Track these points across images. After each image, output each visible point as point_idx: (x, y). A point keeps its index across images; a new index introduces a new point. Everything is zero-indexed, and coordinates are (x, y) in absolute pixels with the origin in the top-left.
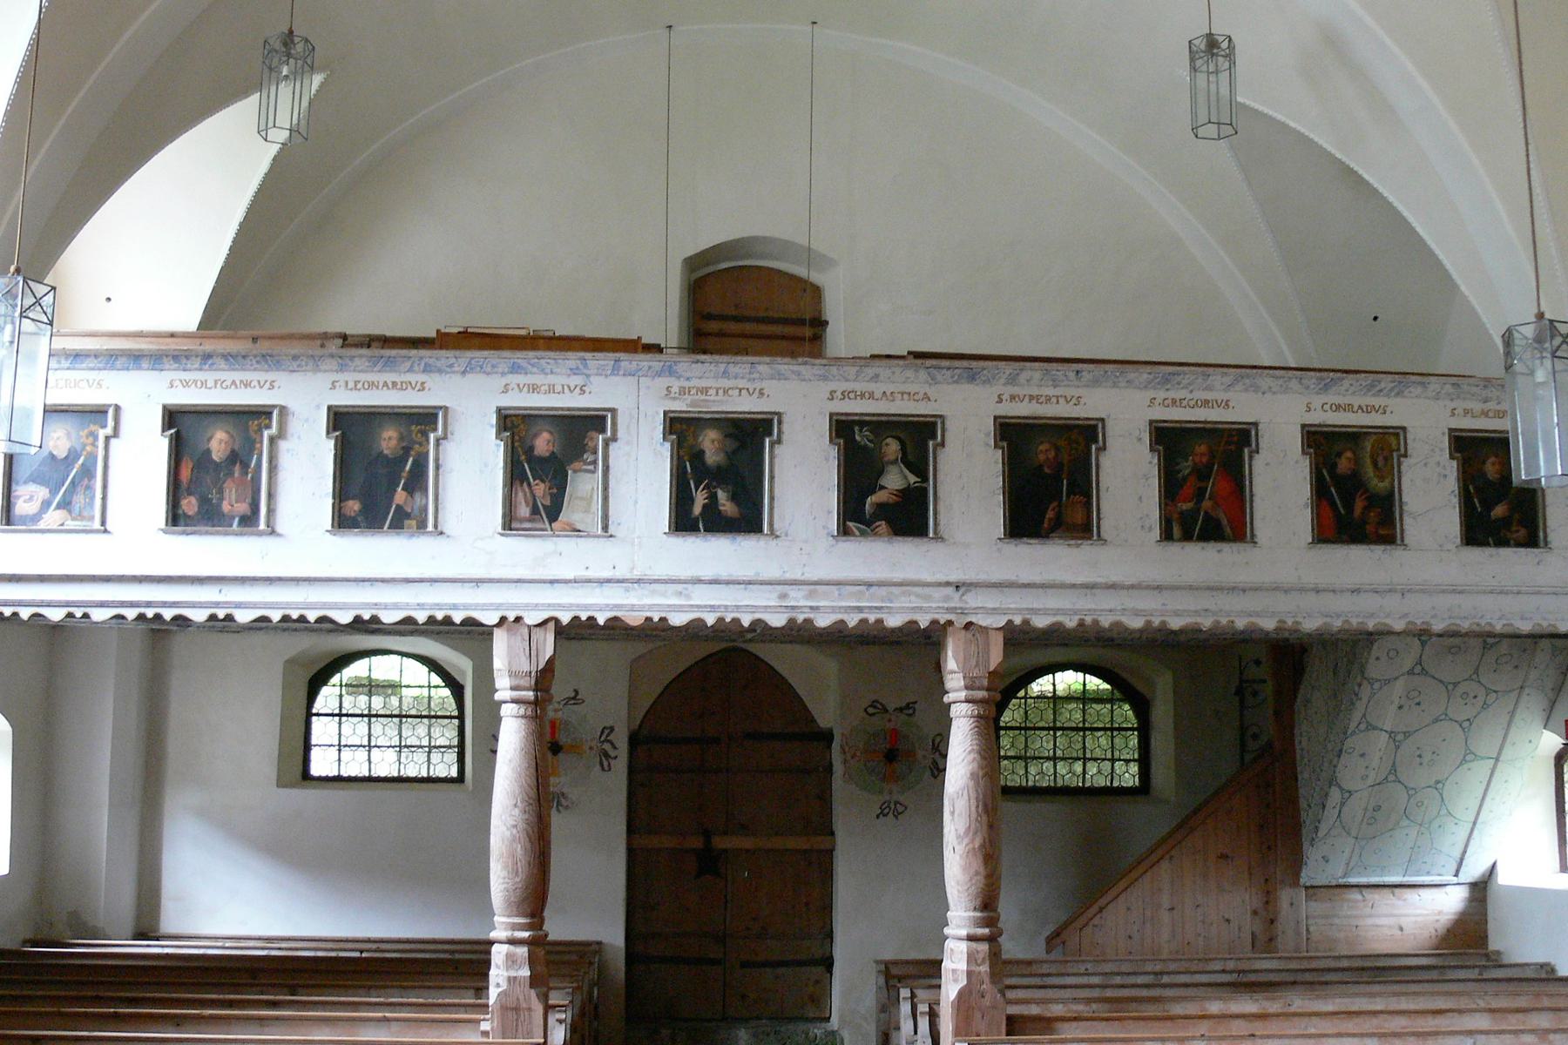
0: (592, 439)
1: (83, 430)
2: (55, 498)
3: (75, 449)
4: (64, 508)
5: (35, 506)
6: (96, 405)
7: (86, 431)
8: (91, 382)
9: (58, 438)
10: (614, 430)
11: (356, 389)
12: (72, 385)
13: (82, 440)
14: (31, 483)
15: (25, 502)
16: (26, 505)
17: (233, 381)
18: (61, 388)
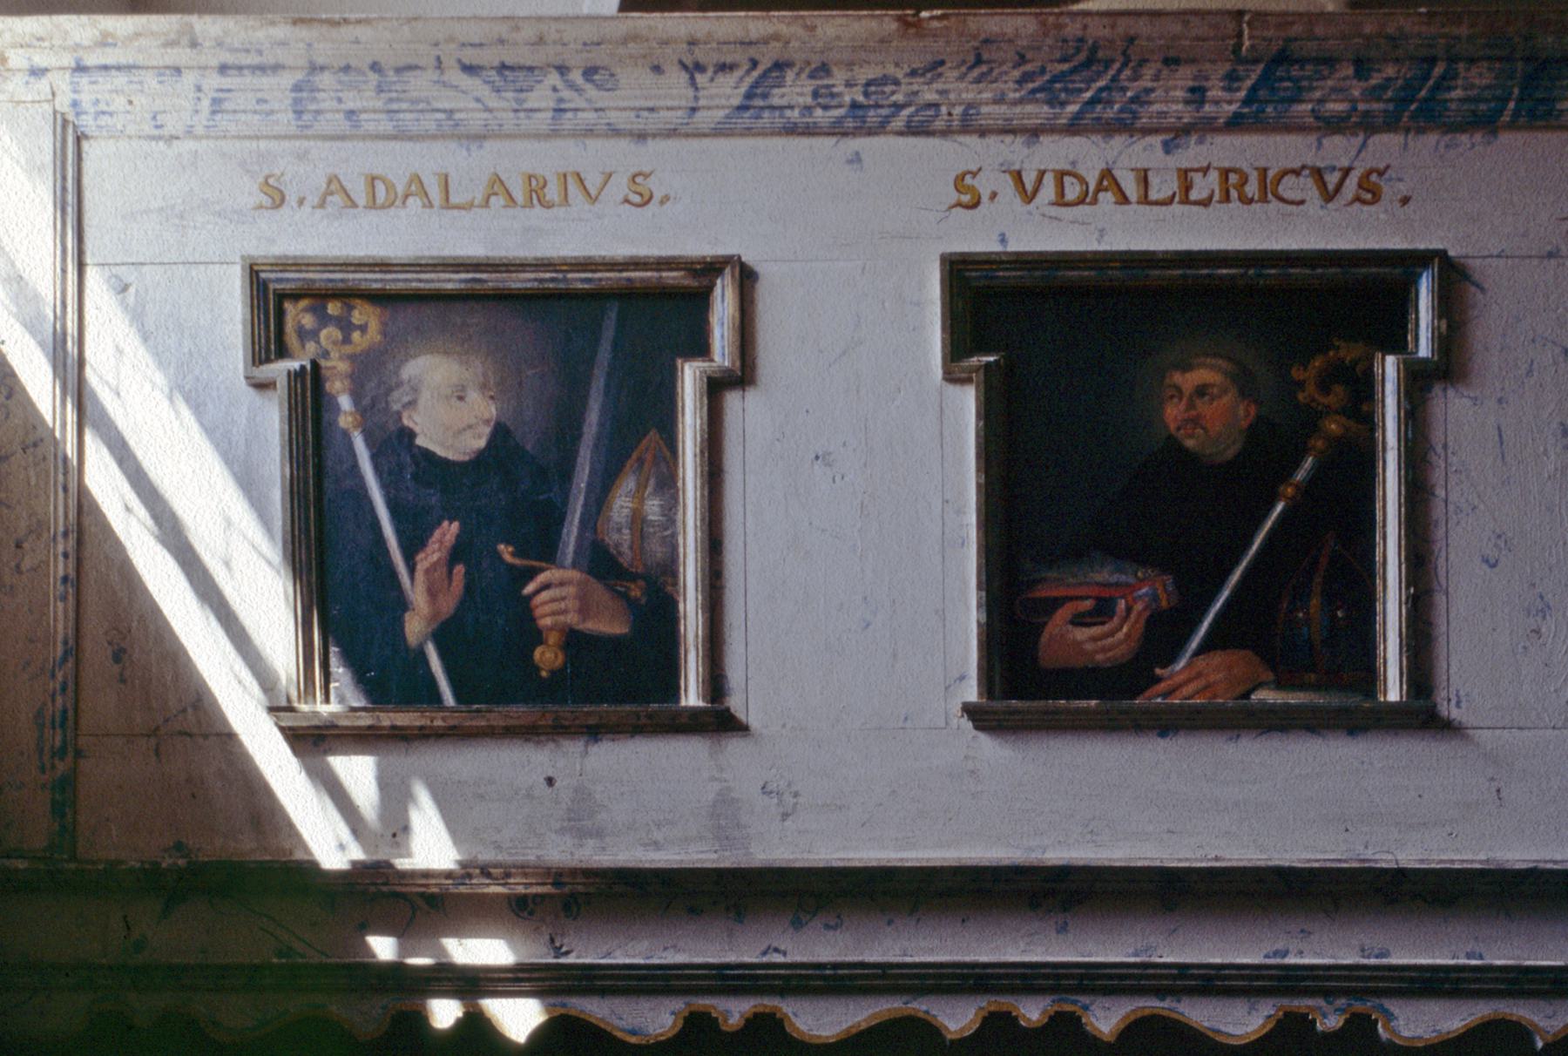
5: (1120, 635)
8: (1332, 179)
9: (1201, 391)
10: (1452, 338)
11: (1186, 201)
12: (1252, 189)
15: (1079, 621)
16: (1081, 634)
17: (1107, 174)
18: (1205, 203)
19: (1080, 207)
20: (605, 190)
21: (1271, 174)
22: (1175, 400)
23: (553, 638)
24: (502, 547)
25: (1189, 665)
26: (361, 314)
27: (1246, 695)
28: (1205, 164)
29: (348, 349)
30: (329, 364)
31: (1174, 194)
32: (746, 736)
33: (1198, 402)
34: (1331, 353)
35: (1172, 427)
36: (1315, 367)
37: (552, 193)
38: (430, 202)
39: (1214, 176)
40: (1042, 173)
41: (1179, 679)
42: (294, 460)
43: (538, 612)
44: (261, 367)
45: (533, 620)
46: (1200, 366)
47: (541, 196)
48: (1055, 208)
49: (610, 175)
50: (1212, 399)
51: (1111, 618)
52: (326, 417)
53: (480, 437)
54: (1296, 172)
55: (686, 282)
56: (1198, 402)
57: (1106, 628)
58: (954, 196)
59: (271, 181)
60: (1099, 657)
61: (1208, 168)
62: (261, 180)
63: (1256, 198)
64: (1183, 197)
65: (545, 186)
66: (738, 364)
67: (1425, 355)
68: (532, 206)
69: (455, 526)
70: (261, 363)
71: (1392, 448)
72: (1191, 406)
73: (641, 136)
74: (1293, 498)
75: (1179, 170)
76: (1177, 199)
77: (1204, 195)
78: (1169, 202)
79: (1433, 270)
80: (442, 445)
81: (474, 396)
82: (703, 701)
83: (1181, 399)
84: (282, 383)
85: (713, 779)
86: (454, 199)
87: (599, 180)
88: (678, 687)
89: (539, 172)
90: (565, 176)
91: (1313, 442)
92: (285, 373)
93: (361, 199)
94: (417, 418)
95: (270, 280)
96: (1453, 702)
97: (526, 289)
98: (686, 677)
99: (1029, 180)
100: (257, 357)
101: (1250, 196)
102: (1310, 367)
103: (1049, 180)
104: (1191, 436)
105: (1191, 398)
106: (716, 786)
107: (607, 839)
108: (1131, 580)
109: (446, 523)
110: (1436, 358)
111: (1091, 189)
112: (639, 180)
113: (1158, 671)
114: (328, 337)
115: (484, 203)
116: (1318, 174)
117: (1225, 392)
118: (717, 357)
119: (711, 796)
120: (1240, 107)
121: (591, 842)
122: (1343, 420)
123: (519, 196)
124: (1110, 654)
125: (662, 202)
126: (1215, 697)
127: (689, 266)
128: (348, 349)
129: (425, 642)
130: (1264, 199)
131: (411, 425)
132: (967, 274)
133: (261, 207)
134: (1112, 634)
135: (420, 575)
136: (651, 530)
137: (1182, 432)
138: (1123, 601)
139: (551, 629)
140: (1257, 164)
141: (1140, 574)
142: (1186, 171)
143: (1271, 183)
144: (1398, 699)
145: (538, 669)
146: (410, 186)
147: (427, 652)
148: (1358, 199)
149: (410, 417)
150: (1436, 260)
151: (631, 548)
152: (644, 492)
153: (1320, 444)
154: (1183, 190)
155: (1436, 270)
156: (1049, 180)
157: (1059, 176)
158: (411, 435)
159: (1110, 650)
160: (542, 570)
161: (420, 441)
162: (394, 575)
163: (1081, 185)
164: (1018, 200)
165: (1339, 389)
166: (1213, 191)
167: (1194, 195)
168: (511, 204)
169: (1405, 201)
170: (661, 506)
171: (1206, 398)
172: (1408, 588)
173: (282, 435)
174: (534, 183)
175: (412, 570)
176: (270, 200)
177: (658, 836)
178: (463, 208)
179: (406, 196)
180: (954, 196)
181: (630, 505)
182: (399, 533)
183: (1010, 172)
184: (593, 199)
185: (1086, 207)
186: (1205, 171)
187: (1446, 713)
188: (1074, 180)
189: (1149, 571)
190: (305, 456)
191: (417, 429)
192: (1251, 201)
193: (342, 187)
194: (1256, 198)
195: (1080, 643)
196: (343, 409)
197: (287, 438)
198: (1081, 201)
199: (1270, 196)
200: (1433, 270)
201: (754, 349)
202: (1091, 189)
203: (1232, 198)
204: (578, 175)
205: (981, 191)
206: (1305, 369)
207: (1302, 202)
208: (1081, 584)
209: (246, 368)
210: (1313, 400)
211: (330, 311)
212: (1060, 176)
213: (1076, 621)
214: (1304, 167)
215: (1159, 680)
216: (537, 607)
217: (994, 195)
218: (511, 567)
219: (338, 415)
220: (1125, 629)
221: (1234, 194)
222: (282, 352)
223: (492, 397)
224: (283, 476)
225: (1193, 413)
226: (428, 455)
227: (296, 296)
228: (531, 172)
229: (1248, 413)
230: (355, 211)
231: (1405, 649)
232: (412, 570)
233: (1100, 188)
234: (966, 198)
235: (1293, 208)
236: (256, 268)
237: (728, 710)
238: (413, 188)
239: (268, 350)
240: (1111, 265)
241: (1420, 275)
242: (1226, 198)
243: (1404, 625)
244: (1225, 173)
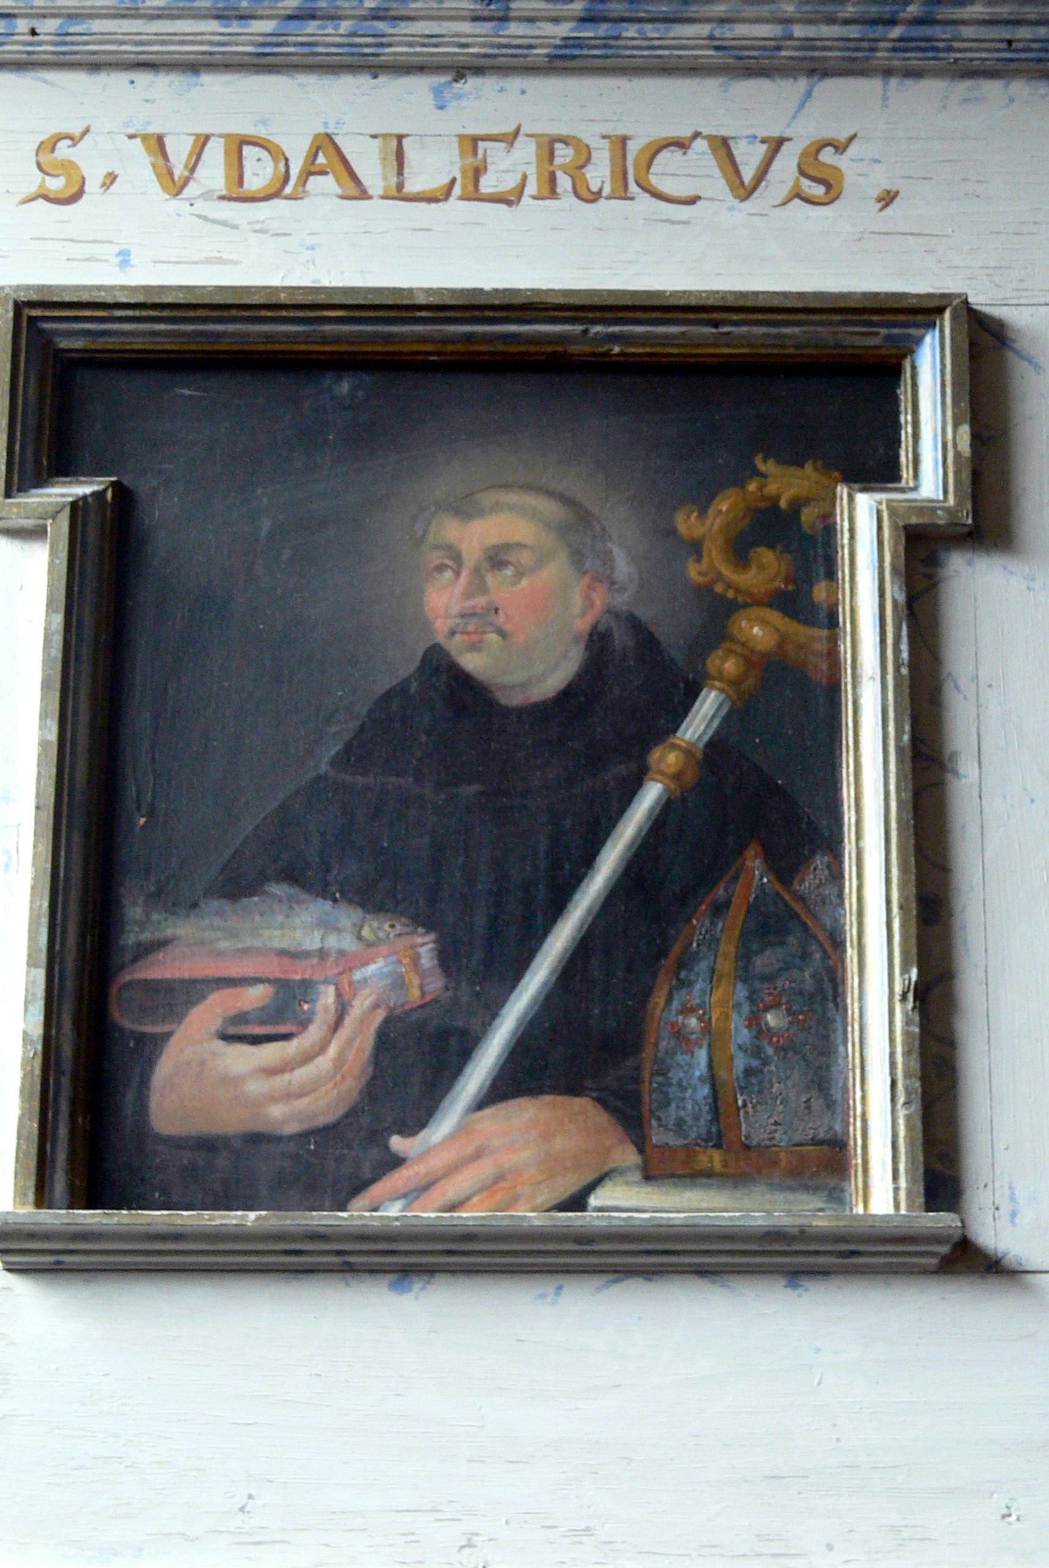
0: (813, 526)
1: (703, 505)
2: (492, 1010)
3: (636, 625)
4: (573, 1090)
5: (324, 1063)
6: (463, 292)
7: (724, 504)
8: (750, 159)
9: (496, 558)
11: (474, 195)
12: (599, 174)
13: (694, 571)
14: (278, 889)
17: (325, 143)
19: (275, 202)
21: (633, 148)
22: (448, 574)
25: (462, 1130)
27: (577, 1202)
28: (510, 128)
31: (454, 181)
33: (491, 579)
34: (752, 487)
35: (441, 626)
36: (720, 511)
39: (526, 152)
40: (203, 141)
41: (437, 1162)
46: (497, 507)
48: (226, 204)
50: (520, 574)
51: (304, 1023)
54: (681, 145)
56: (491, 579)
57: (291, 1048)
58: (34, 180)
60: (277, 1111)
61: (516, 133)
63: (607, 191)
64: (471, 188)
67: (932, 496)
71: (873, 678)
72: (478, 586)
74: (677, 777)
75: (461, 138)
76: (457, 190)
77: (509, 183)
78: (446, 193)
79: (942, 331)
83: (457, 574)
91: (717, 662)
96: (1004, 1212)
97: (94, 676)
99: (179, 151)
101: (594, 189)
102: (711, 512)
103: (215, 152)
104: (475, 647)
105: (477, 571)
108: (348, 943)
110: (951, 501)
111: (295, 171)
113: (397, 1143)
116: (723, 147)
117: (541, 561)
120: (573, 30)
122: (775, 617)
124: (302, 1103)
126: (512, 1202)
130: (622, 193)
132: (46, 326)
134: (307, 1058)
137: (458, 638)
138: (331, 989)
140: (608, 129)
141: (366, 932)
142: (475, 140)
143: (636, 164)
144: (891, 1211)
146: (315, 156)
148: (798, 195)
150: (947, 315)
153: (731, 666)
154: (471, 175)
155: (947, 331)
156: (215, 152)
157: (235, 147)
159: (301, 1094)
163: (276, 161)
164: (155, 187)
165: (766, 556)
166: (525, 178)
167: (488, 184)
169: (887, 199)
171: (509, 572)
172: (905, 970)
180: (34, 180)
183: (145, 138)
185: (283, 202)
186: (510, 139)
187: (993, 1241)
188: (264, 154)
189: (386, 927)
192: (595, 197)
194: (607, 191)
195: (238, 1080)
198: (274, 194)
199: (633, 188)
200: (942, 331)
202: (295, 171)
203: (559, 190)
205: (86, 172)
206: (703, 513)
207: (692, 201)
208: (246, 951)
210: (720, 577)
212: (238, 145)
213: (232, 1031)
214: (697, 135)
215: (396, 1162)
217: (111, 179)
220: (333, 1050)
221: (564, 182)
225: (481, 601)
229: (589, 603)
231: (901, 1099)
233: (310, 171)
234: (55, 184)
235: (684, 212)
238: (321, 159)
240: (673, 342)
241: (919, 341)
242: (551, 190)
243: (899, 1050)
244: (548, 146)
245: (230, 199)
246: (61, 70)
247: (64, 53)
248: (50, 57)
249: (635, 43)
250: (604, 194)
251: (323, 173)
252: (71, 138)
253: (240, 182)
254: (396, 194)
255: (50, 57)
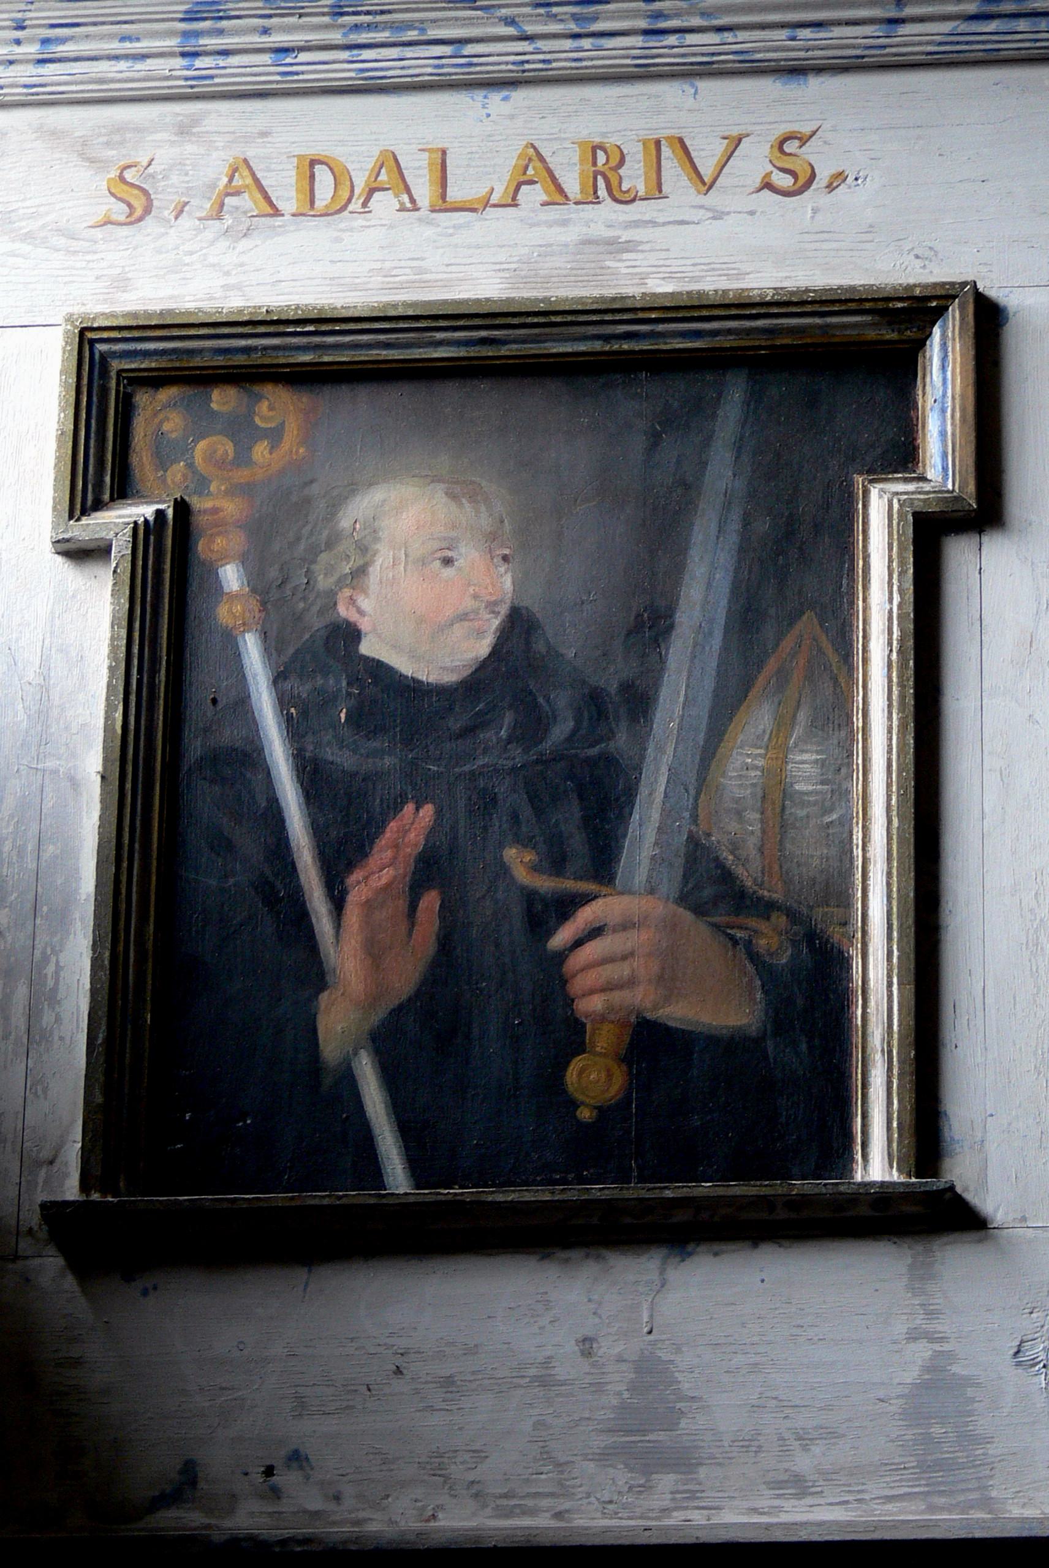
17: (534, 155)
20: (732, 149)
23: (604, 1040)
24: (511, 854)
26: (271, 408)
29: (242, 475)
30: (208, 504)
32: (980, 1241)
37: (634, 176)
38: (413, 200)
42: (133, 698)
43: (577, 985)
44: (85, 521)
45: (570, 1002)
47: (614, 182)
49: (740, 140)
52: (196, 605)
53: (480, 633)
55: (871, 334)
59: (129, 175)
62: (114, 173)
65: (622, 161)
66: (971, 488)
68: (596, 200)
69: (428, 811)
70: (84, 512)
73: (796, 71)
80: (413, 656)
81: (469, 555)
82: (899, 1170)
84: (121, 547)
85: (913, 1336)
86: (454, 193)
87: (720, 147)
88: (848, 1136)
89: (612, 140)
90: (658, 143)
92: (128, 530)
93: (288, 199)
94: (365, 603)
95: (113, 354)
98: (865, 1116)
100: (79, 500)
106: (922, 1351)
107: (702, 1472)
109: (409, 808)
112: (791, 147)
114: (209, 457)
115: (510, 201)
118: (933, 473)
119: (911, 1376)
121: (666, 1481)
123: (572, 184)
125: (831, 187)
127: (881, 305)
128: (242, 475)
129: (356, 1054)
131: (351, 615)
133: (108, 222)
135: (353, 915)
136: (801, 813)
139: (602, 1019)
145: (574, 1104)
146: (378, 175)
147: (357, 1072)
149: (352, 601)
151: (761, 850)
152: (787, 737)
158: (351, 634)
160: (587, 899)
161: (367, 648)
162: (302, 917)
168: (558, 198)
170: (822, 763)
173: (113, 649)
174: (601, 158)
175: (338, 902)
176: (124, 207)
177: (803, 1463)
178: (473, 210)
179: (371, 191)
181: (760, 762)
182: (317, 830)
184: (708, 186)
190: (152, 686)
191: (364, 625)
193: (257, 181)
196: (226, 590)
197: (122, 655)
201: (511, 1253)
204: (681, 141)
209: (55, 526)
211: (214, 406)
216: (574, 976)
218: (530, 897)
219: (217, 603)
222: (123, 490)
223: (505, 558)
224: (108, 729)
226: (378, 669)
227: (156, 381)
228: (597, 140)
230: (278, 221)
232: (338, 902)
236: (90, 335)
237: (952, 1188)
238: (383, 177)
239: (99, 485)
245: (440, 211)
246: (351, 95)
247: (32, 94)
248: (924, 57)
249: (675, 50)
250: (494, 199)
251: (531, 182)
252: (800, 139)
253: (312, 202)
254: (706, 187)
255: (924, 57)
